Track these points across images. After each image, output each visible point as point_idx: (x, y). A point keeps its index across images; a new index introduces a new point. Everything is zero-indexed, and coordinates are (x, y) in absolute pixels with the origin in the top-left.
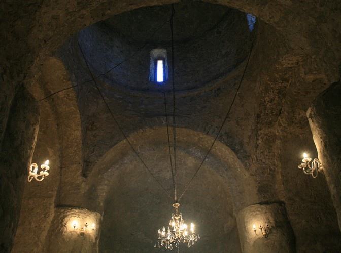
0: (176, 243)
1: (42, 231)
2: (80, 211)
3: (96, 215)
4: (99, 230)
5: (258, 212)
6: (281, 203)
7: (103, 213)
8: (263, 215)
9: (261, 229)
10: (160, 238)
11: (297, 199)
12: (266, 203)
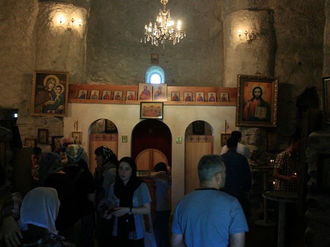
0: (162, 39)
1: (28, 26)
2: (66, 6)
3: (83, 11)
4: (86, 27)
5: (245, 18)
6: (270, 11)
7: (90, 8)
8: (250, 21)
9: (246, 34)
10: (146, 34)
11: (287, 9)
12: (255, 10)
